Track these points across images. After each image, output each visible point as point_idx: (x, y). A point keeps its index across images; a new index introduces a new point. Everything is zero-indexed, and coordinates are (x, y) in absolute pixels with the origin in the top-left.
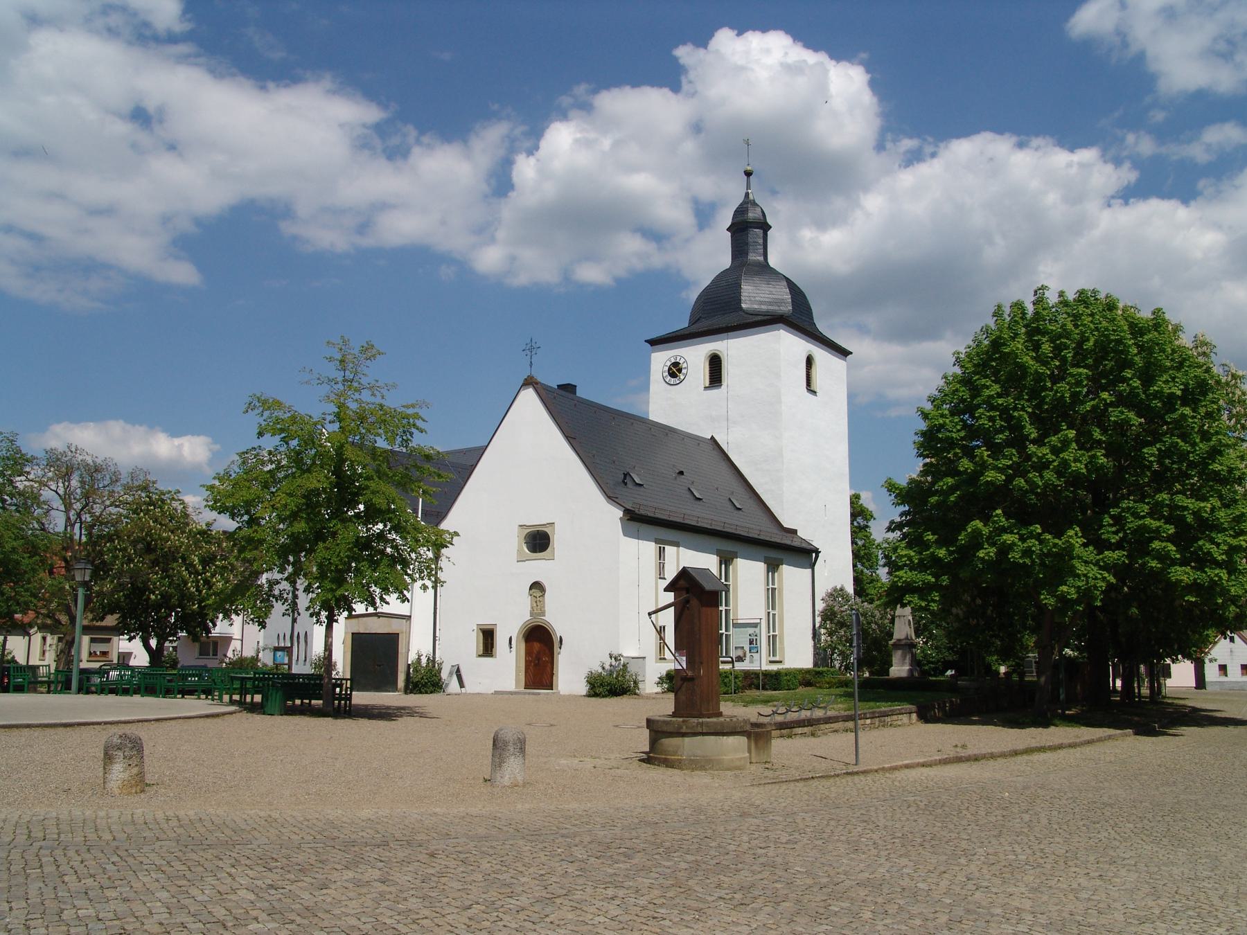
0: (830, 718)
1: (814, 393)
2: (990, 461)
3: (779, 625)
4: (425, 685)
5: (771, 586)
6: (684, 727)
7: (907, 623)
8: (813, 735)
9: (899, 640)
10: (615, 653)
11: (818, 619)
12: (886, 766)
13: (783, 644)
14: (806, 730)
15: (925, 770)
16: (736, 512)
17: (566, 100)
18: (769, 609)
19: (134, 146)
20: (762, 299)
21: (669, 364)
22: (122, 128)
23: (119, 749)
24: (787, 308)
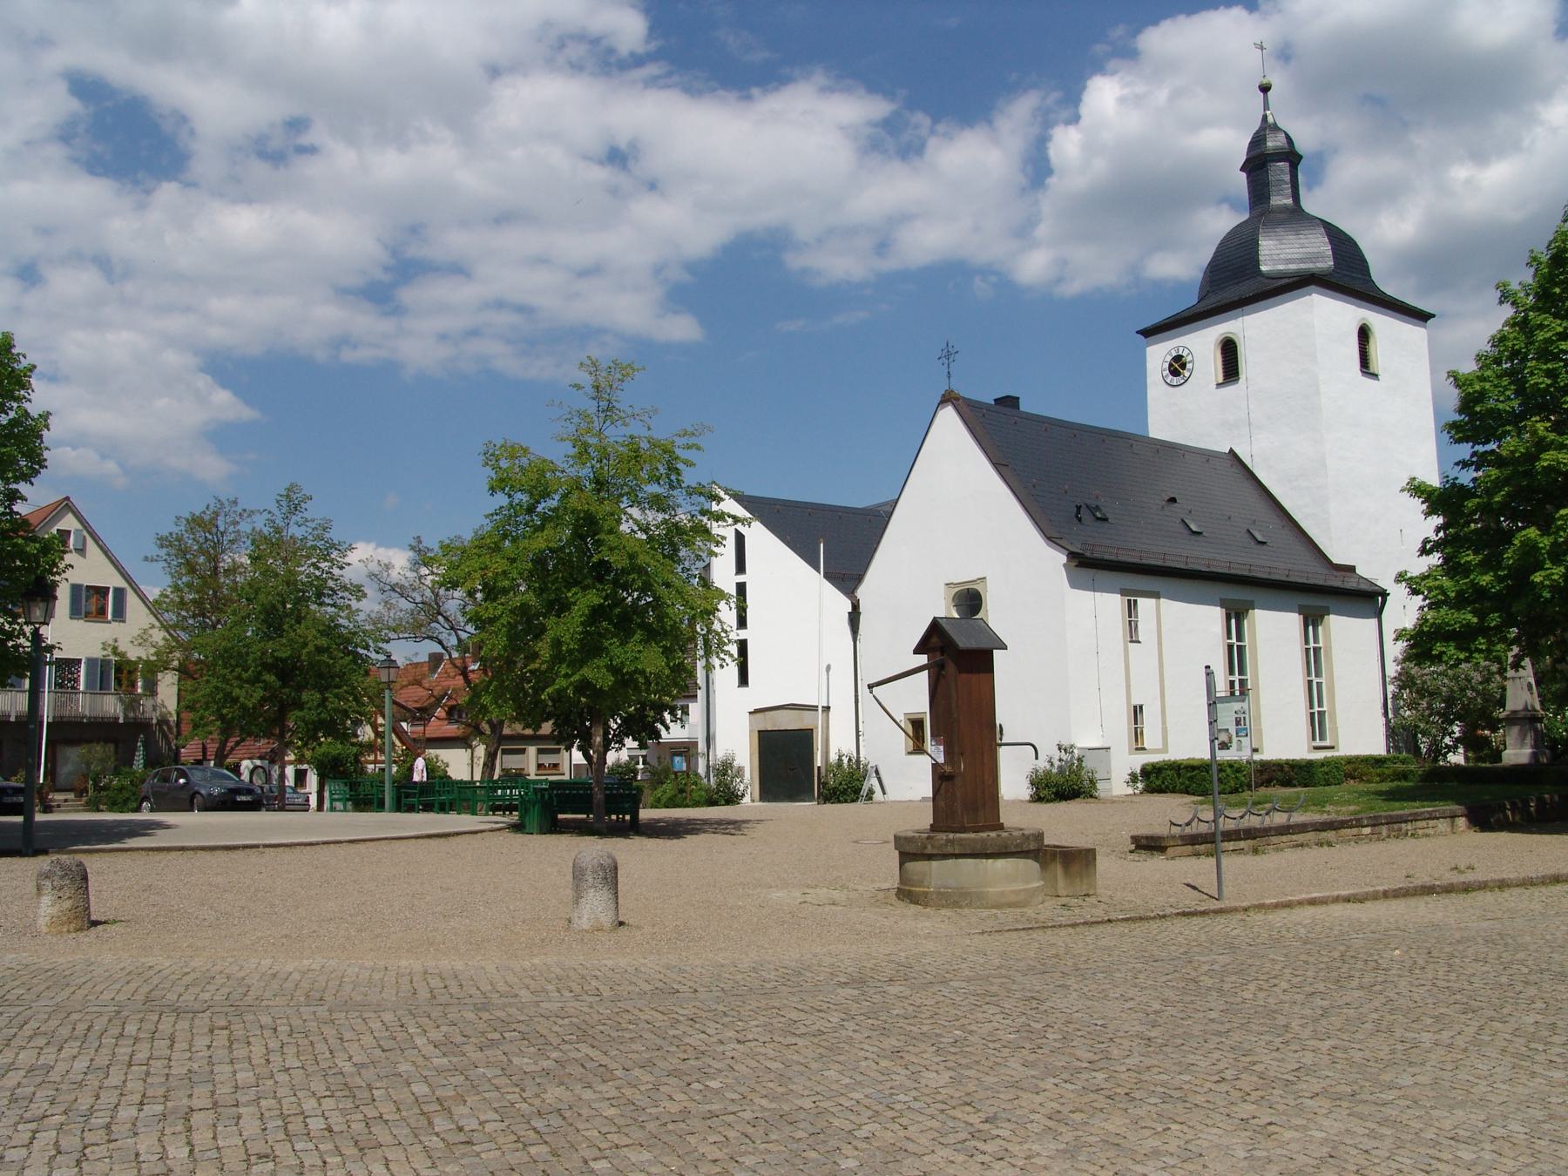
0: (1297, 826)
1: (1375, 376)
2: (1552, 436)
4: (844, 792)
5: (1312, 644)
6: (929, 847)
7: (1525, 687)
8: (1255, 851)
9: (1514, 712)
10: (1065, 743)
12: (1268, 901)
14: (1242, 844)
15: (1398, 907)
16: (1259, 546)
17: (1099, 48)
18: (1309, 674)
19: (614, 191)
20: (1289, 256)
21: (1169, 359)
22: (601, 174)
23: (47, 877)
24: (1327, 263)
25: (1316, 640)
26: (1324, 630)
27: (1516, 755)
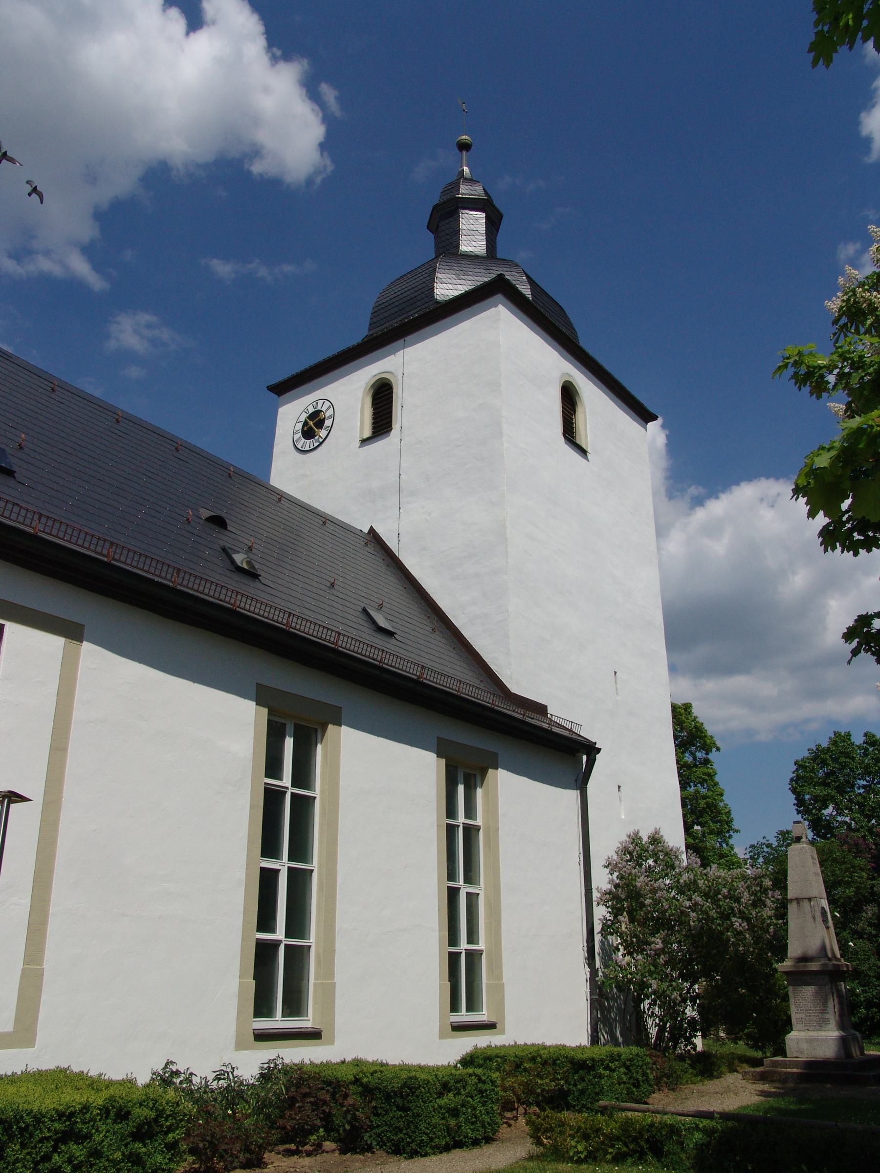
3: (488, 916)
9: (804, 959)
11: (601, 912)
13: (500, 977)
18: (451, 875)
21: (304, 417)
25: (470, 811)
26: (486, 795)
27: (810, 1041)
